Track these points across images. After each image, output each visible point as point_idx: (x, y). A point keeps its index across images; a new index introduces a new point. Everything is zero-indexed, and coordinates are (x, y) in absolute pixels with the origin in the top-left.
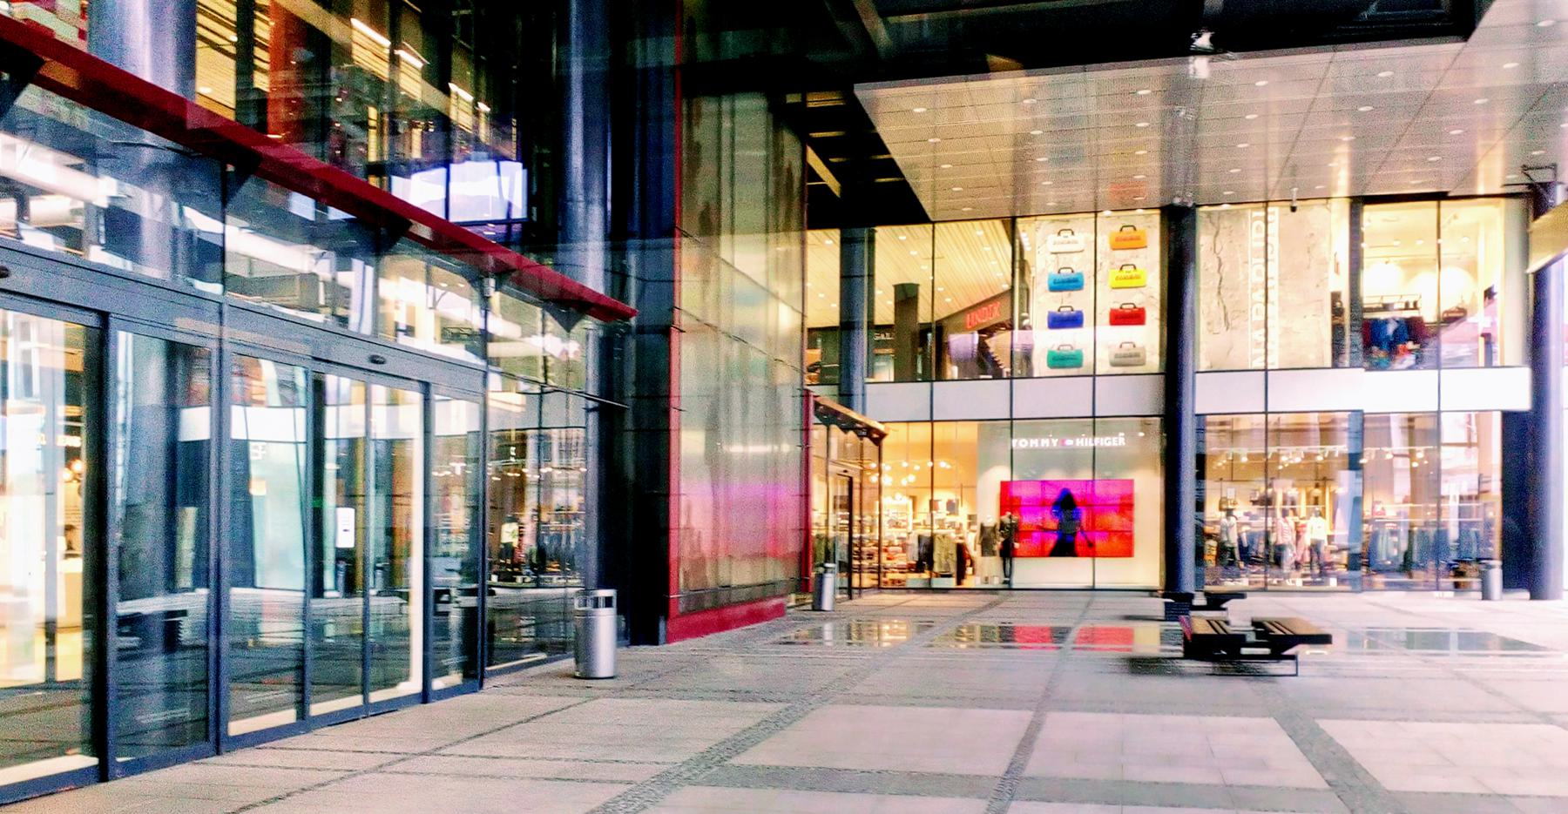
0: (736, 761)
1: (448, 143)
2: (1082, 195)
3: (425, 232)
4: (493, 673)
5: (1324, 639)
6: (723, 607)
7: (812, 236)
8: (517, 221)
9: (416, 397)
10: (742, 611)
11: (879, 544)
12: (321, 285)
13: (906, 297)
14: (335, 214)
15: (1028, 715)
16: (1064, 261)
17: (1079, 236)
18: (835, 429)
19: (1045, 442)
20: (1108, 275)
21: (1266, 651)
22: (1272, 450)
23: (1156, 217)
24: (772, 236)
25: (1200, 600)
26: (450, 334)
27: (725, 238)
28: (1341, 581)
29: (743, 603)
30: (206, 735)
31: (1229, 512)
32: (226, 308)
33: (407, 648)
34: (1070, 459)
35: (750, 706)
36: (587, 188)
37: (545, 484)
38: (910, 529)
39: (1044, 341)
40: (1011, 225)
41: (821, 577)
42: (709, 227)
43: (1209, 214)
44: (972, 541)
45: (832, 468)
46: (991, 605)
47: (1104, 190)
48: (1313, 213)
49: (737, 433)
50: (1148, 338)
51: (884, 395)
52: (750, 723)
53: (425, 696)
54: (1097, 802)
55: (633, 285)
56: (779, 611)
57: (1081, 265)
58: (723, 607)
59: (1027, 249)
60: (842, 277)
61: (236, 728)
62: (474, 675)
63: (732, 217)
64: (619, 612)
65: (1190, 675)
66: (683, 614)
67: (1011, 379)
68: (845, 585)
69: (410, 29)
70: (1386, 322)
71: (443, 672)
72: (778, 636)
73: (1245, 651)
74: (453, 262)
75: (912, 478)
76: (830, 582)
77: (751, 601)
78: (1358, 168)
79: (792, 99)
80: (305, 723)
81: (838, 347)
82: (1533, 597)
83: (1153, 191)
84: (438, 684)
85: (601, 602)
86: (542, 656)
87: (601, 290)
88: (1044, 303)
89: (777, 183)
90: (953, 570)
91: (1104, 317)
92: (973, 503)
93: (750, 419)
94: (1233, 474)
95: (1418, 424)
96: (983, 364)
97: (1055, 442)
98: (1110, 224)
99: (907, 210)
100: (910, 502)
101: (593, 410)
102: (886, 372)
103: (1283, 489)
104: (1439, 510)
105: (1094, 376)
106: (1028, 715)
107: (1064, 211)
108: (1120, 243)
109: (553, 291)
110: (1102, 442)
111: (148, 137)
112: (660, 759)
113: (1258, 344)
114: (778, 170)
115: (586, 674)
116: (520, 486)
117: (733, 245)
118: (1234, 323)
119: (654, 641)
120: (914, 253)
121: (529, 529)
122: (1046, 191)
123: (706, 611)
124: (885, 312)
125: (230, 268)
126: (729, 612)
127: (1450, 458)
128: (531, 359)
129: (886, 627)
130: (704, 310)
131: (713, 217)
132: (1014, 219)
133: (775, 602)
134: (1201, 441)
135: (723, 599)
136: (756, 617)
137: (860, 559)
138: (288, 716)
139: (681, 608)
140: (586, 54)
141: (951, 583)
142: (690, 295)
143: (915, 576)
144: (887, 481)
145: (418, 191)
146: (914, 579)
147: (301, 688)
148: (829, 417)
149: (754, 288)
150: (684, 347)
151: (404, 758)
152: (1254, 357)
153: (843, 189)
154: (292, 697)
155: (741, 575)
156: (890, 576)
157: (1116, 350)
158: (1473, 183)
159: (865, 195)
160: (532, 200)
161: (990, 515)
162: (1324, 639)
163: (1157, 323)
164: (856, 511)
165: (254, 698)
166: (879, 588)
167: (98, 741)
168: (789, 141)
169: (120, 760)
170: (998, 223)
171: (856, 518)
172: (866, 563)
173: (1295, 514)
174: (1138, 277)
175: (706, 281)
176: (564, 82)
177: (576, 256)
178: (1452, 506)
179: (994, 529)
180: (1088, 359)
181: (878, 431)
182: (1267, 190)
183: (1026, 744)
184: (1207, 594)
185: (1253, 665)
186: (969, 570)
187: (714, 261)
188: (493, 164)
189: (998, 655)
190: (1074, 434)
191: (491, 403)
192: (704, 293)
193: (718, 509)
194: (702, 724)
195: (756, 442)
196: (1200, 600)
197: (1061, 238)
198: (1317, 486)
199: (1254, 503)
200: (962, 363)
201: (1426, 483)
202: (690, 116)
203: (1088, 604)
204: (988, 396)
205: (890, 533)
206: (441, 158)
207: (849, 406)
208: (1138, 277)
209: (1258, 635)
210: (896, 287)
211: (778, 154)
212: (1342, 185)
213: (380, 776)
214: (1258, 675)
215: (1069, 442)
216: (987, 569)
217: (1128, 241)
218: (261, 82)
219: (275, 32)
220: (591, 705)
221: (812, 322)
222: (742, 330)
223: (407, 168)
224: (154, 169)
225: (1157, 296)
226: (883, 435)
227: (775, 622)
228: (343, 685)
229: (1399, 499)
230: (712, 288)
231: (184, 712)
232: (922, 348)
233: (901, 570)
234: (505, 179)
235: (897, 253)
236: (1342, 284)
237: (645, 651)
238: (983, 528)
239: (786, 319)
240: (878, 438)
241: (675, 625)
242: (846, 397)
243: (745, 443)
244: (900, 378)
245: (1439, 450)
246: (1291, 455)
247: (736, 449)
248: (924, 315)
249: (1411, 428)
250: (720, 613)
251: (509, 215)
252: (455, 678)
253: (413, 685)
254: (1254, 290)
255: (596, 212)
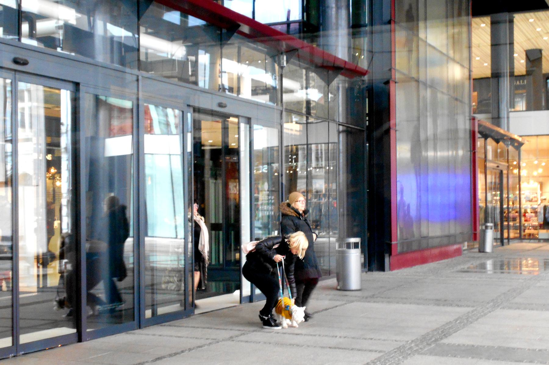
0: (445, 341)
6: (423, 250)
7: (476, 21)
8: (294, 22)
10: (436, 251)
11: (520, 212)
12: (190, 63)
14: (194, 21)
27: (421, 24)
29: (436, 247)
32: (140, 78)
35: (449, 309)
37: (309, 178)
38: (539, 202)
41: (484, 232)
45: (489, 165)
52: (451, 319)
56: (458, 252)
58: (423, 250)
60: (492, 45)
63: (426, 13)
64: (363, 252)
66: (402, 253)
68: (499, 236)
74: (260, 46)
75: (540, 171)
76: (490, 235)
77: (441, 246)
81: (488, 89)
100: (539, 186)
101: (343, 131)
102: (521, 105)
109: (318, 60)
112: (398, 338)
117: (426, 28)
119: (382, 268)
120: (538, 29)
123: (414, 252)
124: (520, 64)
126: (427, 253)
128: (299, 103)
129: (524, 262)
130: (409, 70)
131: (414, 11)
133: (455, 247)
135: (424, 245)
136: (444, 255)
137: (508, 221)
139: (399, 249)
142: (401, 61)
144: (524, 173)
150: (397, 93)
155: (434, 230)
156: (527, 231)
164: (505, 192)
166: (521, 238)
169: (88, 330)
171: (505, 196)
172: (511, 223)
175: (410, 51)
177: (332, 40)
181: (517, 141)
187: (415, 39)
189: (160, 337)
191: (285, 131)
192: (409, 60)
193: (423, 189)
194: (426, 318)
195: (442, 150)
205: (526, 205)
207: (499, 125)
210: (540, 51)
213: (232, 343)
220: (349, 306)
222: (433, 81)
226: (521, 144)
230: (414, 55)
237: (377, 275)
239: (456, 73)
240: (518, 145)
241: (394, 259)
242: (497, 119)
243: (435, 149)
244: (529, 109)
247: (431, 154)
250: (421, 254)
251: (288, 19)
255: (343, 13)
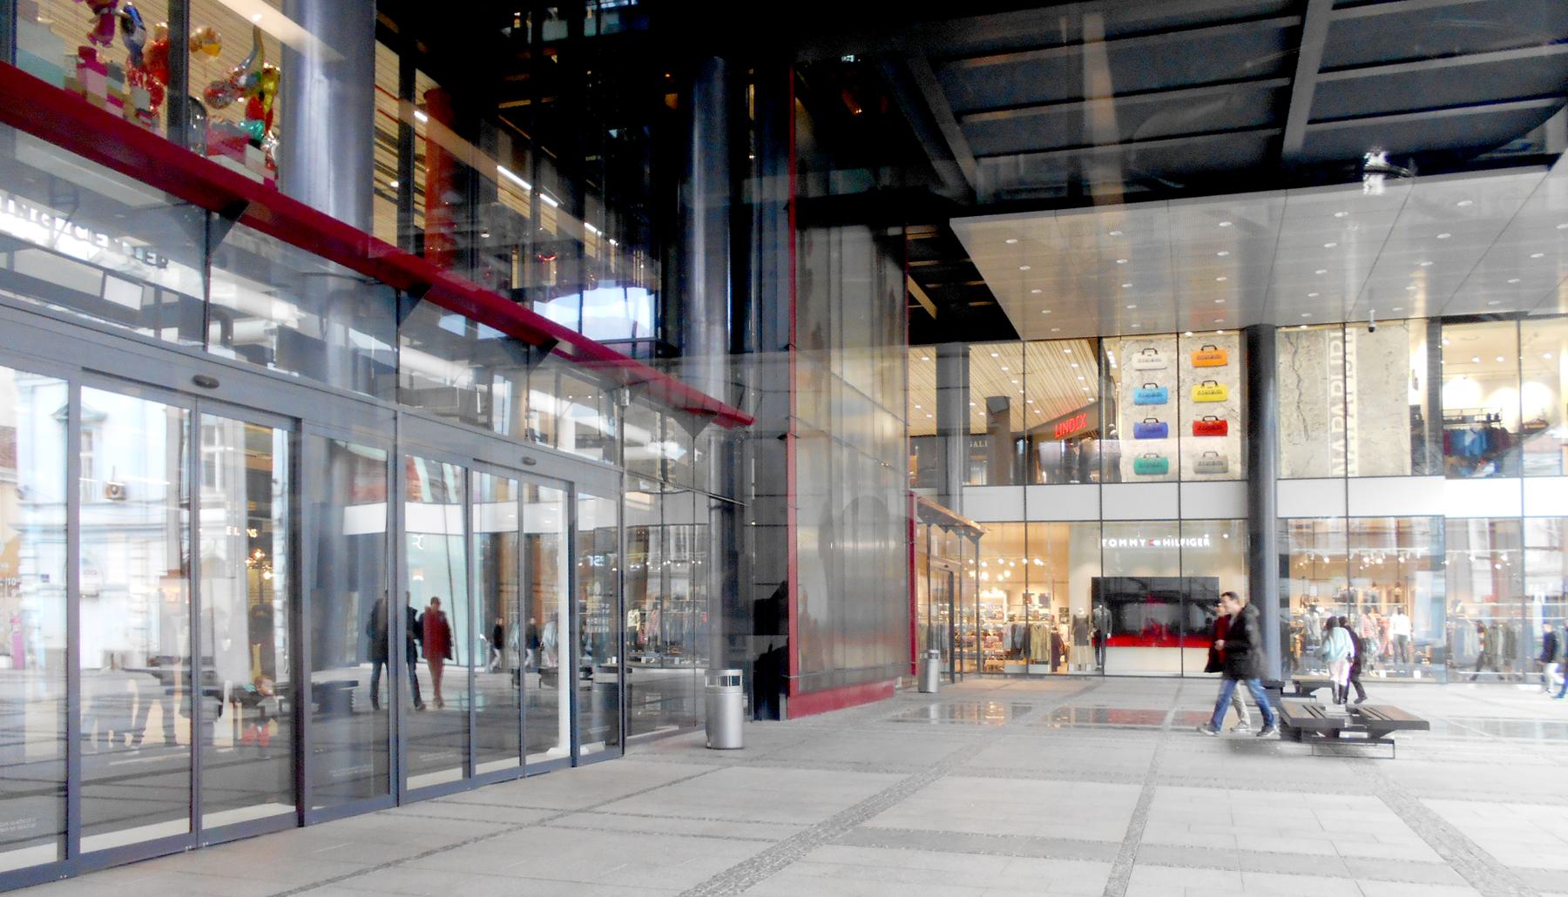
0: (868, 824)
1: (582, 272)
2: (1164, 318)
3: (566, 347)
4: (636, 742)
5: (1422, 725)
8: (643, 340)
9: (560, 494)
10: (855, 691)
13: (999, 409)
14: (485, 332)
15: (1136, 790)
16: (1147, 377)
17: (1161, 355)
18: (935, 528)
19: (1133, 542)
20: (1192, 390)
21: (1365, 735)
22: (1354, 551)
23: (1236, 338)
24: (877, 351)
25: (1289, 688)
26: (586, 438)
27: (835, 353)
28: (1425, 673)
30: (387, 786)
31: (1313, 609)
33: (555, 718)
34: (1159, 557)
36: (709, 311)
37: (666, 576)
39: (1129, 449)
40: (1097, 344)
41: (926, 663)
42: (821, 343)
43: (1287, 335)
44: (1064, 630)
45: (933, 563)
46: (1088, 689)
47: (1185, 314)
48: (1390, 334)
49: (848, 530)
50: (1230, 446)
51: (984, 501)
53: (574, 760)
54: (1217, 868)
55: (751, 395)
56: (889, 692)
57: (1166, 381)
59: (1113, 365)
61: (413, 782)
62: (616, 739)
65: (1290, 756)
67: (1101, 483)
68: (948, 669)
69: (548, 173)
70: (1464, 432)
71: (588, 740)
72: (890, 715)
73: (1343, 735)
74: (588, 373)
75: (1008, 574)
76: (935, 667)
77: (864, 683)
78: (1435, 288)
79: (894, 231)
80: (470, 779)
81: (933, 449)
82: (162, 578)
83: (1236, 317)
84: (584, 750)
85: (730, 681)
86: (675, 728)
87: (721, 398)
88: (1127, 418)
89: (881, 307)
90: (1048, 657)
91: (1188, 428)
92: (1065, 596)
93: (860, 517)
94: (1316, 571)
95: (1499, 529)
96: (1076, 469)
97: (1143, 542)
98: (1191, 344)
99: (997, 327)
102: (980, 477)
103: (1362, 588)
104: (1524, 610)
105: (1179, 482)
106: (1136, 790)
107: (1147, 334)
108: (1203, 361)
110: (1190, 542)
111: (332, 267)
113: (1337, 454)
114: (881, 295)
115: (715, 744)
116: (642, 578)
117: (841, 358)
118: (1314, 435)
119: (775, 715)
121: (653, 616)
122: (1129, 311)
124: (979, 418)
125: (404, 383)
127: (1533, 559)
132: (1099, 339)
134: (1283, 542)
136: (867, 697)
138: (456, 774)
140: (709, 190)
141: (1048, 669)
142: (804, 407)
143: (1013, 662)
144: (984, 576)
145: (557, 311)
146: (1012, 666)
147: (467, 750)
148: (931, 516)
149: (867, 397)
151: (563, 813)
152: (1335, 466)
153: (938, 312)
154: (460, 758)
157: (1199, 458)
158: (1555, 304)
159: (961, 314)
160: (661, 322)
161: (1082, 606)
162: (1422, 725)
163: (1238, 434)
164: (957, 603)
165: (428, 757)
167: (297, 794)
168: (893, 273)
170: (1085, 343)
171: (956, 609)
173: (1376, 611)
174: (1219, 392)
176: (685, 215)
177: (701, 370)
178: (1537, 606)
179: (1087, 621)
180: (1173, 467)
181: (975, 530)
182: (1344, 313)
183: (1140, 813)
184: (1296, 683)
185: (1352, 747)
186: (1062, 658)
188: (620, 290)
190: (1161, 535)
191: (627, 503)
196: (1289, 688)
197: (1146, 356)
198: (1398, 585)
199: (1337, 600)
200: (1050, 470)
201: (1509, 583)
202: (802, 245)
203: (1179, 690)
204: (1076, 500)
205: (988, 624)
206: (576, 282)
207: (948, 506)
208: (1219, 392)
209: (1355, 720)
211: (881, 280)
212: (1420, 306)
214: (1356, 757)
215: (1157, 543)
216: (1082, 656)
217: (1209, 360)
218: (419, 221)
219: (429, 178)
221: (916, 428)
223: (547, 295)
224: (338, 295)
225: (1238, 410)
226: (980, 534)
227: (890, 701)
228: (499, 750)
229: (1477, 599)
231: (369, 768)
232: (1018, 454)
233: (1000, 657)
234: (631, 304)
235: (990, 366)
236: (1419, 397)
237: (768, 725)
238: (1076, 621)
239: (886, 426)
242: (945, 496)
243: (855, 539)
244: (990, 484)
245: (1523, 554)
246: (1373, 556)
248: (1016, 424)
249: (1492, 532)
250: (832, 696)
252: (599, 746)
253: (562, 749)
254: (1333, 404)
